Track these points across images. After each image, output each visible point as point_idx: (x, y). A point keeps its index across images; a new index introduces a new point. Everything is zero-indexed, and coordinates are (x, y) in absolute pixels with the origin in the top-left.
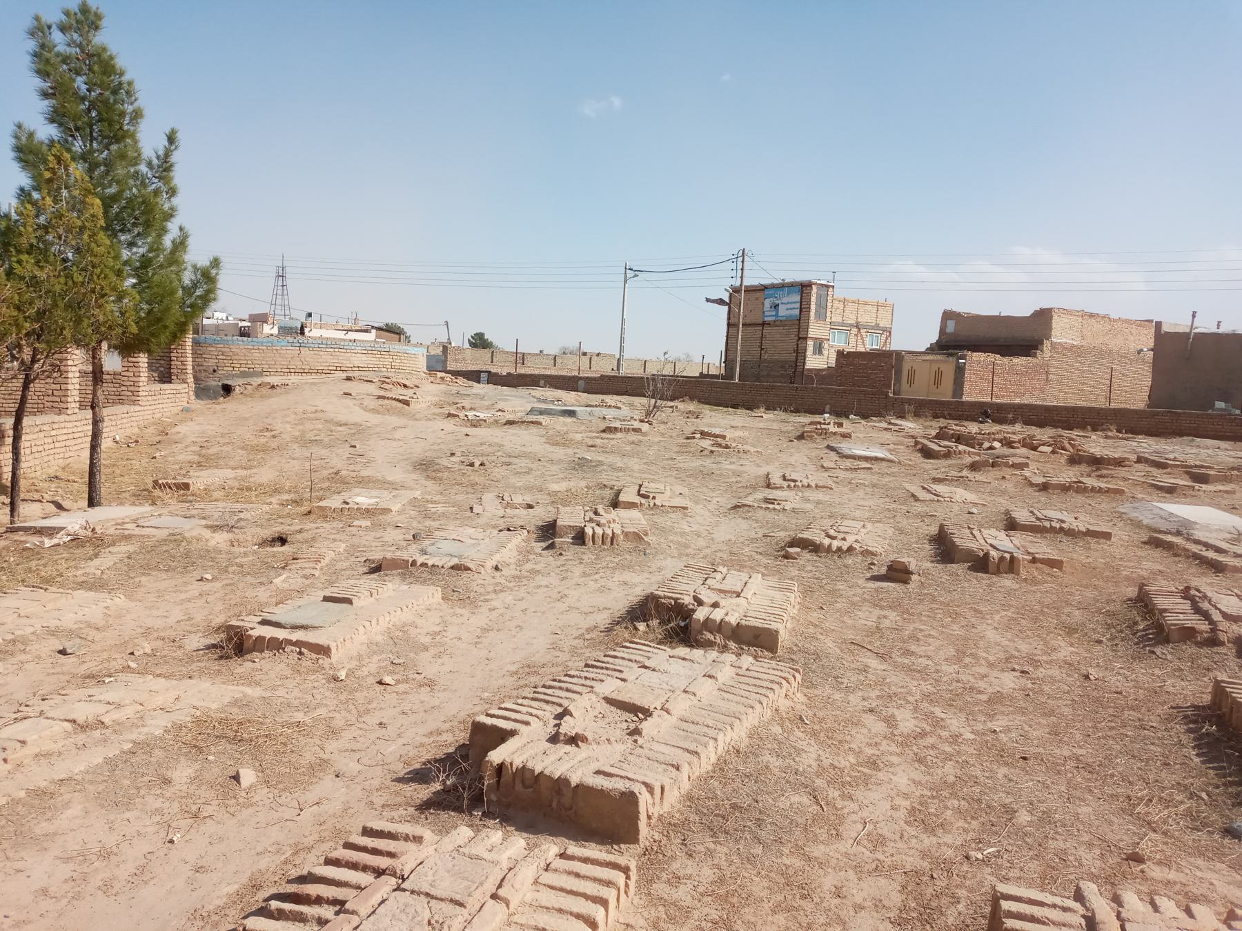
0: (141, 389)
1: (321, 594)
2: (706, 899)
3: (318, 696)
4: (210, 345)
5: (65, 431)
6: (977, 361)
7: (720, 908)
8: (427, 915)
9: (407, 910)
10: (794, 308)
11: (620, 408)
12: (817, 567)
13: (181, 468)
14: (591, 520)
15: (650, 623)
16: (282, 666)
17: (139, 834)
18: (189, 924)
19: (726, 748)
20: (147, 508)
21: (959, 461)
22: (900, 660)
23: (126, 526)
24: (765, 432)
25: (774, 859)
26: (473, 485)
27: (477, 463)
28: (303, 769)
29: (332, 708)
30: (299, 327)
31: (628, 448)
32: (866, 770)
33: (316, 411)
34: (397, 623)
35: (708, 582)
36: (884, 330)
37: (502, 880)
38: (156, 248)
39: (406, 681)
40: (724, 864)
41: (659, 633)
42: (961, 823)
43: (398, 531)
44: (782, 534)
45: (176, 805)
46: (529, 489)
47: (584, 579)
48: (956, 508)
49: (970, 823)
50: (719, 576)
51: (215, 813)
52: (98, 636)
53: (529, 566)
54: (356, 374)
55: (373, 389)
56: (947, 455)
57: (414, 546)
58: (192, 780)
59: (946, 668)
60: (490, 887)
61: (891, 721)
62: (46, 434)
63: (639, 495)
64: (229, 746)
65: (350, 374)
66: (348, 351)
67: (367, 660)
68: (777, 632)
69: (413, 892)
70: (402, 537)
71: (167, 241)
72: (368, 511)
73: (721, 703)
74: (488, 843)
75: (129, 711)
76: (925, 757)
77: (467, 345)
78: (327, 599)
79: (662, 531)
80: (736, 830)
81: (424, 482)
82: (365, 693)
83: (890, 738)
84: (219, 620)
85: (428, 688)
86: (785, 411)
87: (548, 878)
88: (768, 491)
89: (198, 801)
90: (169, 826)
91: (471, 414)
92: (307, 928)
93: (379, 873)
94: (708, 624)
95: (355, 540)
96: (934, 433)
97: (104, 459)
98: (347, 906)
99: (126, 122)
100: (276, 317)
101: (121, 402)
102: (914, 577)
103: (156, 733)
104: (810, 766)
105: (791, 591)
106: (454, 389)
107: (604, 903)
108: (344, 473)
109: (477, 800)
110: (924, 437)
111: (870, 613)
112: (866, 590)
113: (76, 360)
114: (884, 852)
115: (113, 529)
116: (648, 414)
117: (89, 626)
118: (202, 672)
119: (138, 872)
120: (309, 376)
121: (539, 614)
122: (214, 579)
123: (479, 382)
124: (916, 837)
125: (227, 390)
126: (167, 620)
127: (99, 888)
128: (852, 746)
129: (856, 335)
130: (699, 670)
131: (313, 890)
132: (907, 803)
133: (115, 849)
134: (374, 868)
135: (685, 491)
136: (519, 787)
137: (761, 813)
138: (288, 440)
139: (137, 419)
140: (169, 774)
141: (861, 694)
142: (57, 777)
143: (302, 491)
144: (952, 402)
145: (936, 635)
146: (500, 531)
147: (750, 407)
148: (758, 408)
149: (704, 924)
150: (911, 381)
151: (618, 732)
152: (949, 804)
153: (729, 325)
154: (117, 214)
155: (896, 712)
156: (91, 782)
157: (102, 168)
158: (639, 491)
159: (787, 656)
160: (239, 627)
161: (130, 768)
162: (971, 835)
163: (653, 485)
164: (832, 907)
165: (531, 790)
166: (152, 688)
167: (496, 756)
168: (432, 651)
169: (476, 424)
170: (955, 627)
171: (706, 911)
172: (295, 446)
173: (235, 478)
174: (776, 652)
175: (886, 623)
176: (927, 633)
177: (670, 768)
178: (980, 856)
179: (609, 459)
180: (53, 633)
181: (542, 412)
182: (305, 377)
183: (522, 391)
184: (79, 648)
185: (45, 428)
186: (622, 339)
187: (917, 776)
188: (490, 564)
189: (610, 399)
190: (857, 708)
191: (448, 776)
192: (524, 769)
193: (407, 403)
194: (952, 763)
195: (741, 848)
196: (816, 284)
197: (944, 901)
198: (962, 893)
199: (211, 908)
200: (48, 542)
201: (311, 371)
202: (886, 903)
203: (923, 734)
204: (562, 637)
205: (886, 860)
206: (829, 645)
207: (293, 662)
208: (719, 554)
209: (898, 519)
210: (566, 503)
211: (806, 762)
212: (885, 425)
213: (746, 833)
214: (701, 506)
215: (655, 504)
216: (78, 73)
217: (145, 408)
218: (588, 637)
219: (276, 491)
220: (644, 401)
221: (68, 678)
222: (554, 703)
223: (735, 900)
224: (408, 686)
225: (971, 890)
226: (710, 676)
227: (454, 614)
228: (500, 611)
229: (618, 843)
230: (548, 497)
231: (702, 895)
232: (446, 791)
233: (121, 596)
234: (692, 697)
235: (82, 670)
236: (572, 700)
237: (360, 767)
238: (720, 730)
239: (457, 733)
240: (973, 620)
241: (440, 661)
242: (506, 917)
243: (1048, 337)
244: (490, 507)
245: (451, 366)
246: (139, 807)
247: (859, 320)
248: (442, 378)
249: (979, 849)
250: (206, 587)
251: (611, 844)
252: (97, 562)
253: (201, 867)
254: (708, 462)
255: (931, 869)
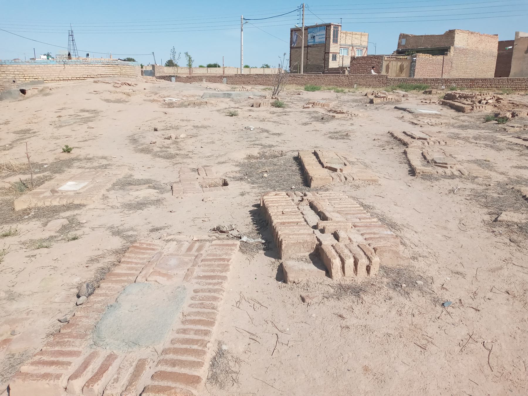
6: (421, 58)
10: (323, 38)
54: (100, 79)
66: (94, 65)
129: (352, 50)
201: (72, 79)
243: (452, 43)
247: (353, 43)
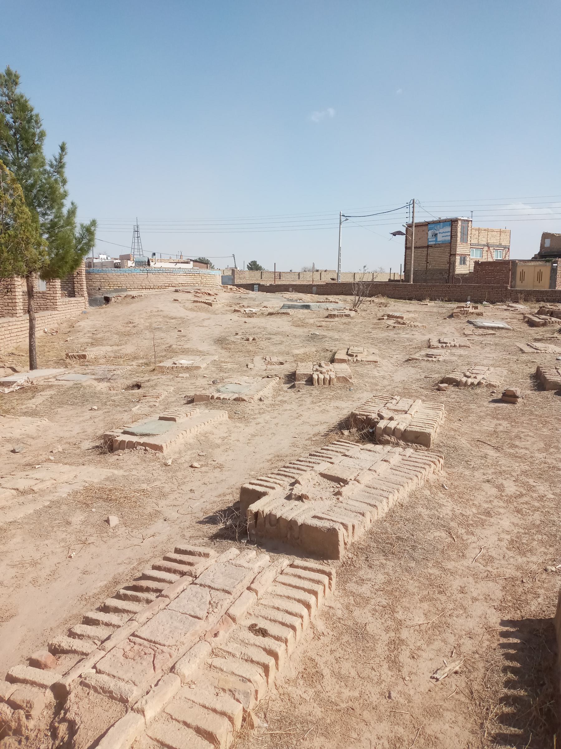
0: (58, 301)
1: (158, 416)
2: (379, 593)
3: (156, 475)
4: (96, 274)
5: (16, 327)
7: (388, 598)
8: (208, 598)
9: (197, 595)
10: (447, 236)
11: (337, 303)
12: (458, 395)
13: (81, 346)
14: (317, 370)
15: (351, 430)
16: (135, 457)
17: (52, 552)
18: (78, 603)
19: (394, 504)
20: (62, 370)
21: (552, 328)
22: (508, 451)
23: (50, 380)
24: (429, 314)
25: (422, 570)
26: (249, 352)
27: (251, 339)
28: (145, 517)
29: (164, 481)
30: (147, 261)
31: (342, 327)
32: (483, 517)
33: (158, 311)
34: (202, 432)
35: (387, 405)
36: (505, 247)
37: (254, 579)
38: (58, 216)
39: (207, 465)
40: (391, 572)
41: (357, 436)
42: (543, 549)
43: (205, 379)
44: (437, 376)
45: (74, 536)
46: (281, 353)
47: (312, 405)
48: (548, 357)
49: (548, 549)
50: (394, 402)
51: (95, 541)
52: (32, 442)
53: (280, 398)
54: (181, 288)
55: (191, 297)
56: (544, 325)
57: (213, 388)
58: (83, 523)
59: (537, 455)
60: (246, 583)
61: (500, 488)
62: (5, 328)
63: (347, 354)
64: (104, 503)
65: (177, 288)
67: (184, 454)
68: (430, 434)
69: (201, 585)
70: (206, 383)
71: (65, 211)
72: (187, 368)
73: (392, 477)
74: (248, 558)
75: (48, 484)
76: (521, 509)
77: (246, 269)
78: (161, 419)
79: (362, 376)
80: (399, 552)
81: (220, 351)
82: (183, 472)
83: (500, 497)
84: (100, 432)
85: (219, 469)
86: (442, 300)
87: (282, 578)
88: (428, 350)
89: (86, 534)
90: (69, 548)
91: (247, 310)
92: (140, 605)
93: (183, 574)
94: (386, 430)
95: (180, 385)
96: (536, 311)
97: (37, 343)
98: (163, 593)
99: (36, 140)
100: (135, 256)
101: (47, 309)
102: (519, 400)
103: (63, 496)
104: (447, 514)
105: (440, 410)
106: (238, 295)
107: (315, 593)
108: (174, 346)
109: (244, 534)
110: (530, 314)
111: (491, 422)
112: (488, 409)
113: (20, 285)
114: (492, 566)
115: (42, 382)
116: (355, 305)
117: (28, 436)
118: (90, 462)
119: (51, 574)
120: (153, 291)
121: (285, 426)
122: (99, 409)
123: (253, 291)
124: (513, 558)
125: (107, 300)
126: (71, 432)
127: (30, 582)
128: (475, 502)
130: (379, 457)
131: (144, 583)
132: (508, 537)
133: (39, 561)
134: (180, 572)
135: (376, 351)
136: (268, 526)
137: (415, 542)
138: (142, 328)
139: (57, 318)
140: (70, 519)
141: (482, 471)
142: (8, 521)
143: (150, 358)
144: (548, 291)
145: (532, 435)
146: (263, 378)
147: (420, 299)
148: (425, 299)
149: (377, 607)
150: (522, 279)
151: (328, 493)
152: (535, 537)
153: (406, 248)
154: (35, 196)
155: (504, 482)
156: (27, 523)
157: (24, 169)
158: (347, 352)
159: (436, 449)
160: (110, 435)
161: (48, 516)
162: (549, 557)
163: (356, 348)
164: (458, 598)
165: (275, 527)
166: (62, 471)
167: (254, 507)
168: (222, 448)
169: (251, 315)
170: (544, 430)
171: (379, 599)
172: (146, 332)
173: (112, 351)
174: (429, 447)
175: (501, 428)
176: (526, 434)
177: (359, 515)
178: (554, 569)
179: (330, 334)
180: (9, 441)
181: (290, 307)
182: (151, 291)
183: (278, 295)
184: (22, 449)
185: (5, 325)
186: (339, 260)
187: (516, 521)
188: (256, 397)
189: (331, 298)
190: (479, 480)
191: (227, 520)
192: (270, 515)
193: (210, 304)
194: (539, 512)
195: (402, 563)
196: (460, 220)
197: (530, 596)
198: (541, 591)
199: (91, 594)
200: (7, 390)
202: (492, 597)
203: (521, 495)
204: (298, 439)
205: (493, 571)
206: (463, 442)
207: (142, 455)
208: (397, 389)
209: (511, 364)
210: (302, 360)
211: (445, 512)
212: (505, 307)
213: (405, 554)
214: (386, 360)
215: (357, 360)
216: (7, 112)
217: (61, 312)
218: (314, 439)
219: (135, 358)
220: (352, 297)
221: (16, 466)
222: (289, 476)
223: (397, 594)
224: (207, 468)
225: (547, 589)
226: (385, 461)
227: (236, 427)
228: (262, 425)
229: (327, 559)
230: (292, 358)
231: (377, 590)
232: (226, 528)
233: (46, 419)
234: (374, 473)
235: (24, 461)
236: (301, 475)
237: (178, 515)
238: (390, 492)
239: (235, 495)
240: (556, 425)
241: (226, 454)
242: (256, 600)
244: (258, 364)
245: (237, 281)
246: (53, 537)
248: (231, 289)
249: (554, 565)
250: (94, 413)
251: (323, 560)
252: (33, 400)
253: (87, 571)
254: (391, 334)
255: (522, 577)
